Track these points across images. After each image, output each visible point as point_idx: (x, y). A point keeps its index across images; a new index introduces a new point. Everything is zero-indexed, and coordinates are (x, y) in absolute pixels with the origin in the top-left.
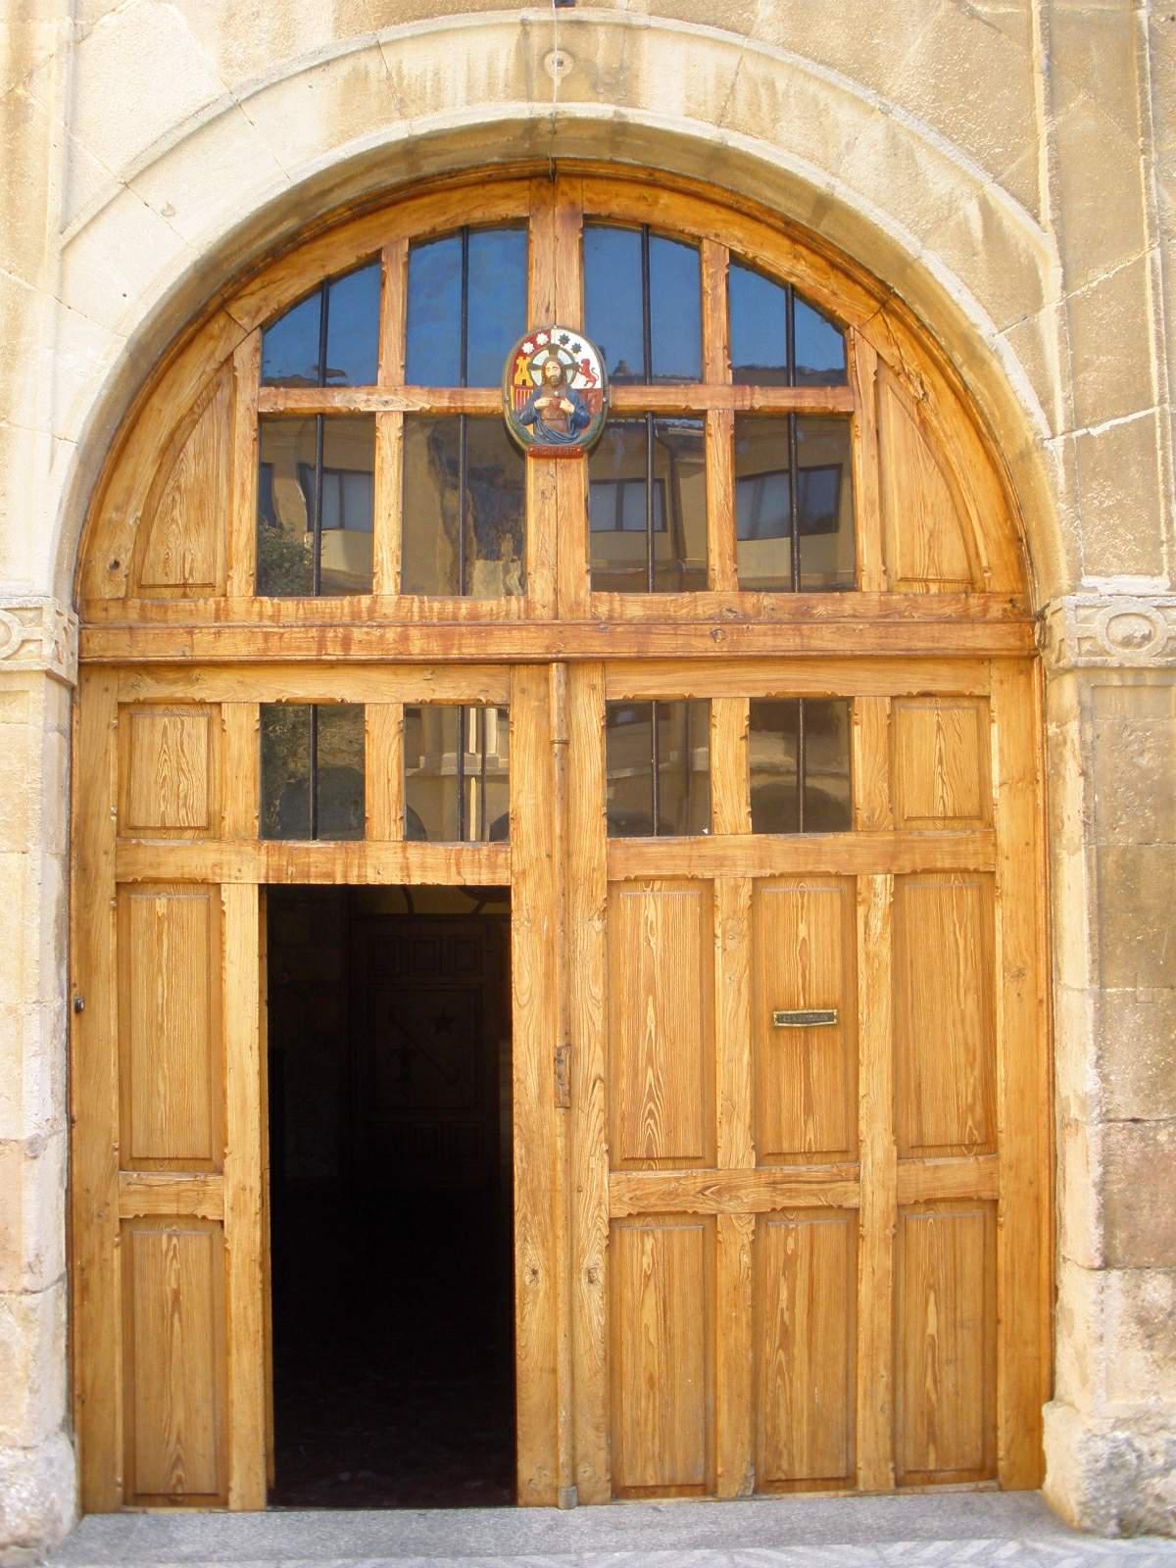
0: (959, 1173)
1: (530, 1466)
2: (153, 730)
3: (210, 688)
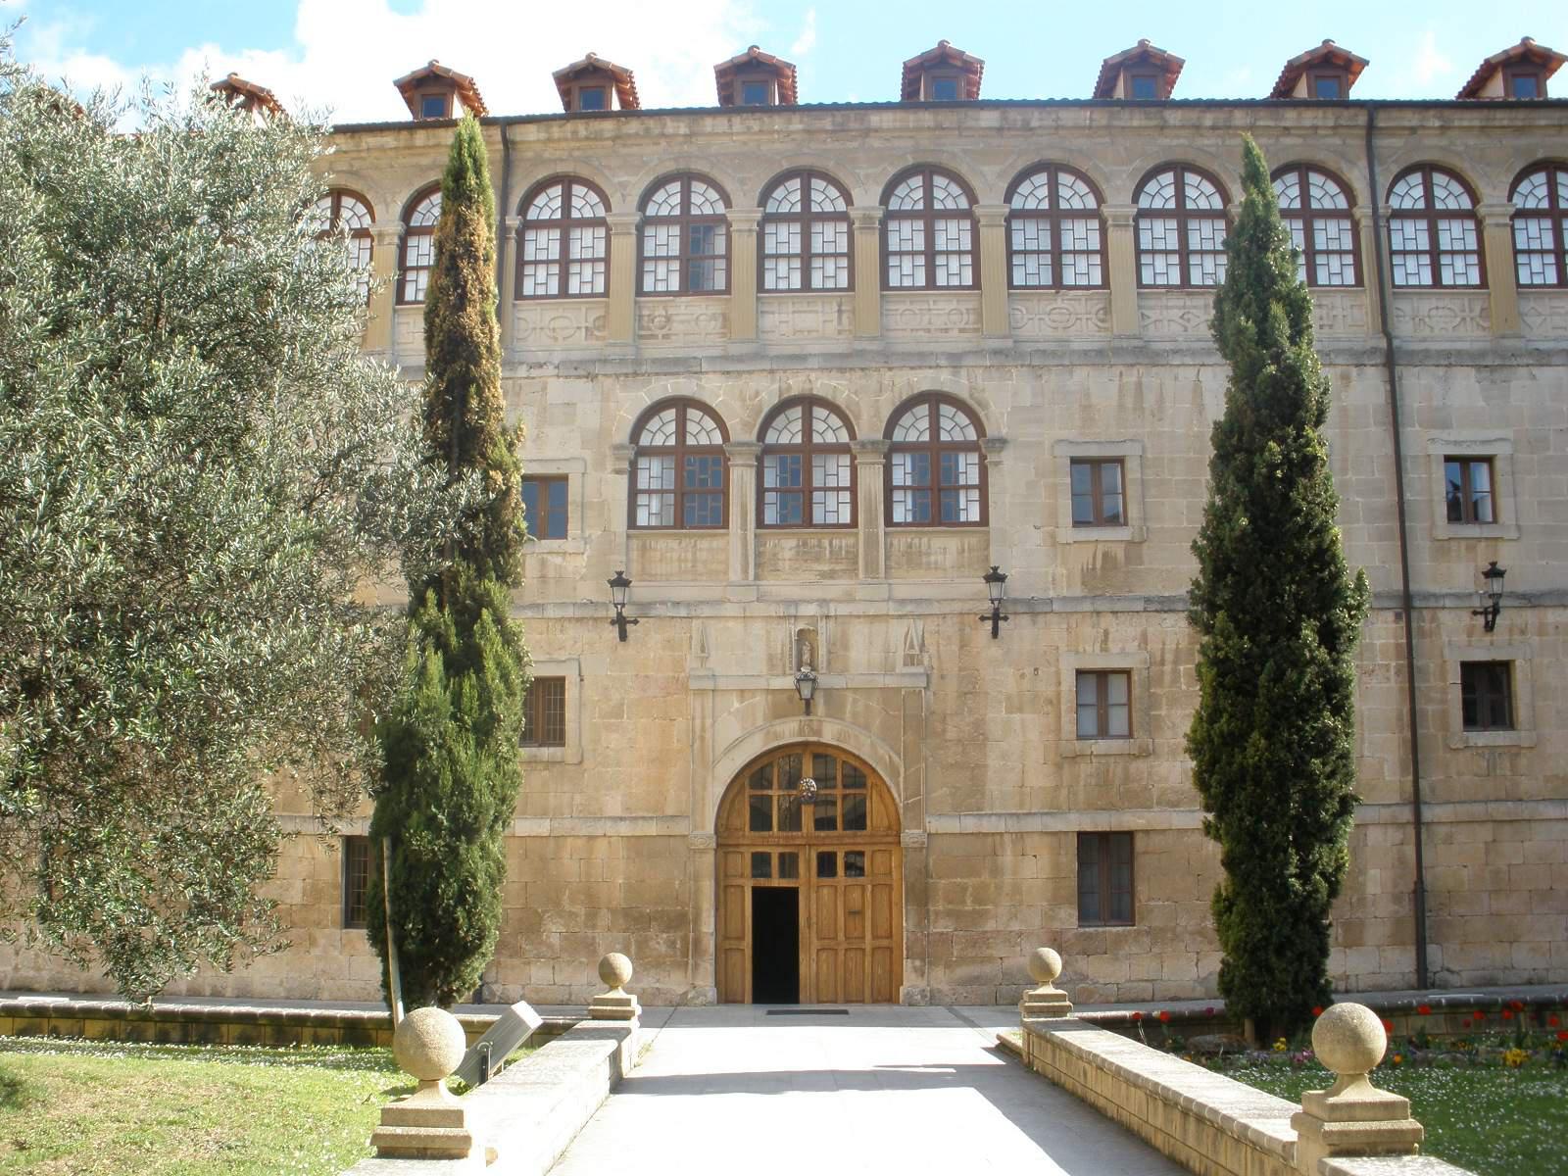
0: (885, 943)
1: (801, 997)
2: (731, 857)
3: (742, 849)
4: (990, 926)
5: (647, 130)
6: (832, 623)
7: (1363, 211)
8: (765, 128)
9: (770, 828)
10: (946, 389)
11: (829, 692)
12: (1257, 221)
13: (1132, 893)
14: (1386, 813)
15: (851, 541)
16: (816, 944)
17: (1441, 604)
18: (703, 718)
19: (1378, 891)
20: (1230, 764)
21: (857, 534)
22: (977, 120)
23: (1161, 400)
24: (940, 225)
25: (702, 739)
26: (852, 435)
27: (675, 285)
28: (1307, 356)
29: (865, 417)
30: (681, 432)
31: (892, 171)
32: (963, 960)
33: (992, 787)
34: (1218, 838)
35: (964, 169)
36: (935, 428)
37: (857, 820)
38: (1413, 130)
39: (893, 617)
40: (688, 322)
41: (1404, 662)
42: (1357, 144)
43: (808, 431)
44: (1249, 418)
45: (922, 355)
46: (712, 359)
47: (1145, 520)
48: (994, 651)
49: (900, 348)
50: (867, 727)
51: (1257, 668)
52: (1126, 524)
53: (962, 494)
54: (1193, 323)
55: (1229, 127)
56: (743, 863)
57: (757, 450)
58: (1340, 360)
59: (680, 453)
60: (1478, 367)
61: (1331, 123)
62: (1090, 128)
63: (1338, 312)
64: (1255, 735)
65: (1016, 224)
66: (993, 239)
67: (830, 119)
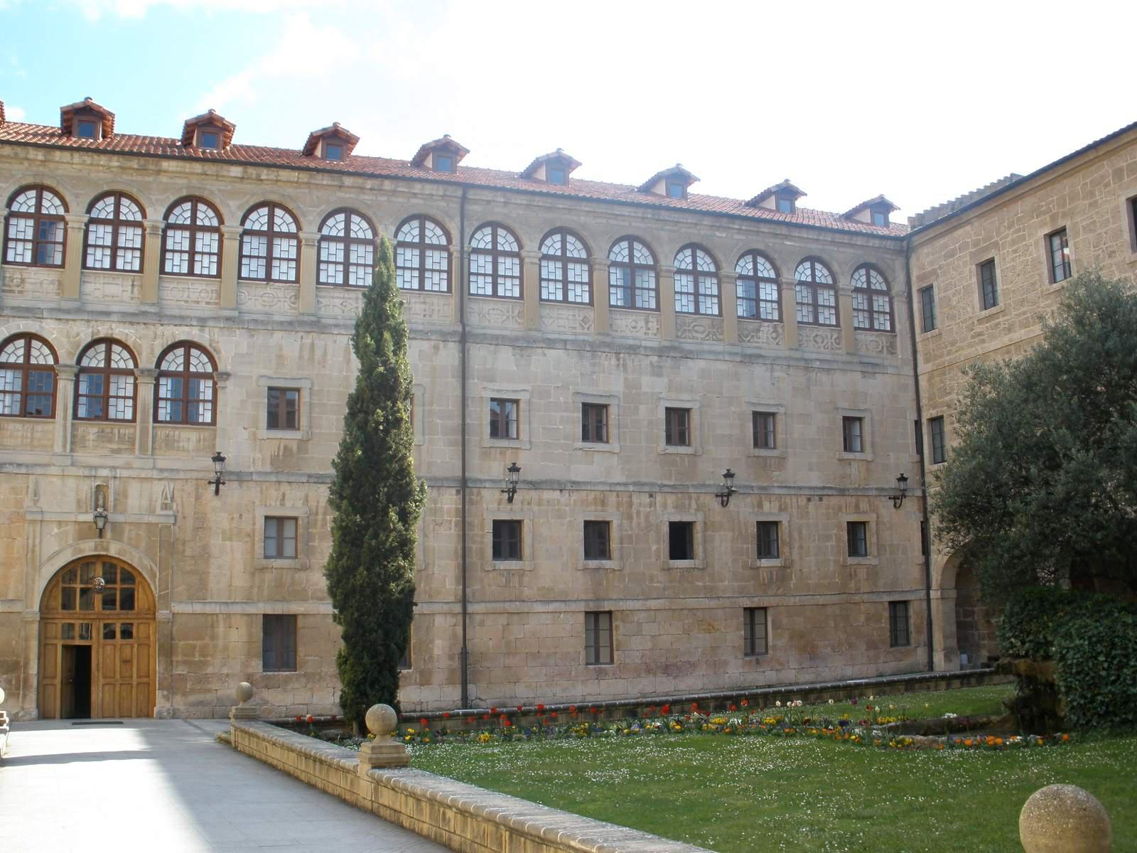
0: (145, 680)
2: (49, 626)
3: (56, 621)
4: (210, 670)
5: (16, 154)
6: (117, 482)
7: (455, 248)
8: (95, 163)
9: (74, 608)
10: (196, 340)
11: (114, 524)
12: (383, 283)
13: (295, 651)
14: (446, 607)
15: (132, 430)
16: (102, 681)
17: (483, 485)
18: (34, 538)
19: (440, 653)
20: (347, 583)
21: (135, 427)
22: (229, 171)
23: (325, 354)
24: (199, 235)
25: (33, 551)
26: (136, 365)
27: (28, 259)
28: (401, 363)
29: (144, 354)
30: (28, 355)
31: (173, 198)
32: (193, 691)
33: (212, 585)
34: (340, 623)
35: (217, 202)
36: (187, 363)
37: (128, 601)
38: (488, 202)
39: (156, 479)
40: (35, 283)
41: (460, 519)
42: (455, 207)
43: (108, 359)
44: (367, 395)
45: (182, 318)
46: (52, 310)
47: (311, 427)
48: (216, 502)
49: (169, 312)
50: (136, 547)
51: (364, 532)
52: (299, 429)
53: (201, 405)
54: (349, 308)
55: (380, 190)
56: (56, 629)
57: (76, 370)
58: (433, 337)
59: (26, 368)
60: (514, 347)
61: (441, 193)
62: (297, 182)
63: (436, 308)
64: (361, 569)
65: (246, 239)
66: (231, 247)
67: (136, 161)
